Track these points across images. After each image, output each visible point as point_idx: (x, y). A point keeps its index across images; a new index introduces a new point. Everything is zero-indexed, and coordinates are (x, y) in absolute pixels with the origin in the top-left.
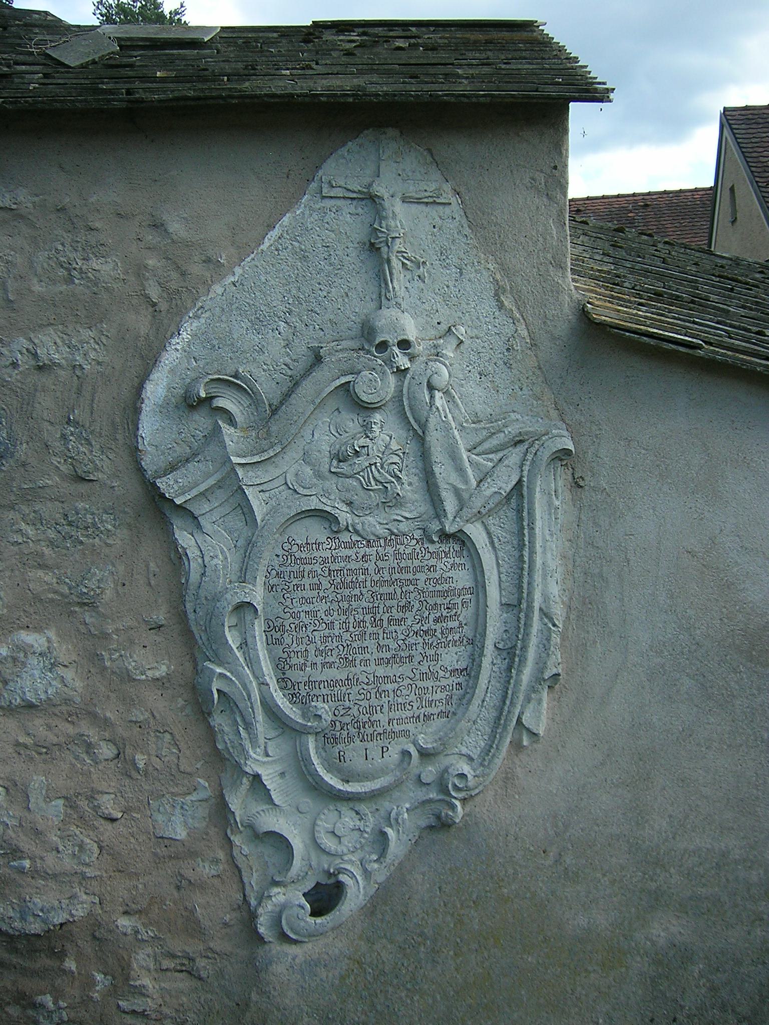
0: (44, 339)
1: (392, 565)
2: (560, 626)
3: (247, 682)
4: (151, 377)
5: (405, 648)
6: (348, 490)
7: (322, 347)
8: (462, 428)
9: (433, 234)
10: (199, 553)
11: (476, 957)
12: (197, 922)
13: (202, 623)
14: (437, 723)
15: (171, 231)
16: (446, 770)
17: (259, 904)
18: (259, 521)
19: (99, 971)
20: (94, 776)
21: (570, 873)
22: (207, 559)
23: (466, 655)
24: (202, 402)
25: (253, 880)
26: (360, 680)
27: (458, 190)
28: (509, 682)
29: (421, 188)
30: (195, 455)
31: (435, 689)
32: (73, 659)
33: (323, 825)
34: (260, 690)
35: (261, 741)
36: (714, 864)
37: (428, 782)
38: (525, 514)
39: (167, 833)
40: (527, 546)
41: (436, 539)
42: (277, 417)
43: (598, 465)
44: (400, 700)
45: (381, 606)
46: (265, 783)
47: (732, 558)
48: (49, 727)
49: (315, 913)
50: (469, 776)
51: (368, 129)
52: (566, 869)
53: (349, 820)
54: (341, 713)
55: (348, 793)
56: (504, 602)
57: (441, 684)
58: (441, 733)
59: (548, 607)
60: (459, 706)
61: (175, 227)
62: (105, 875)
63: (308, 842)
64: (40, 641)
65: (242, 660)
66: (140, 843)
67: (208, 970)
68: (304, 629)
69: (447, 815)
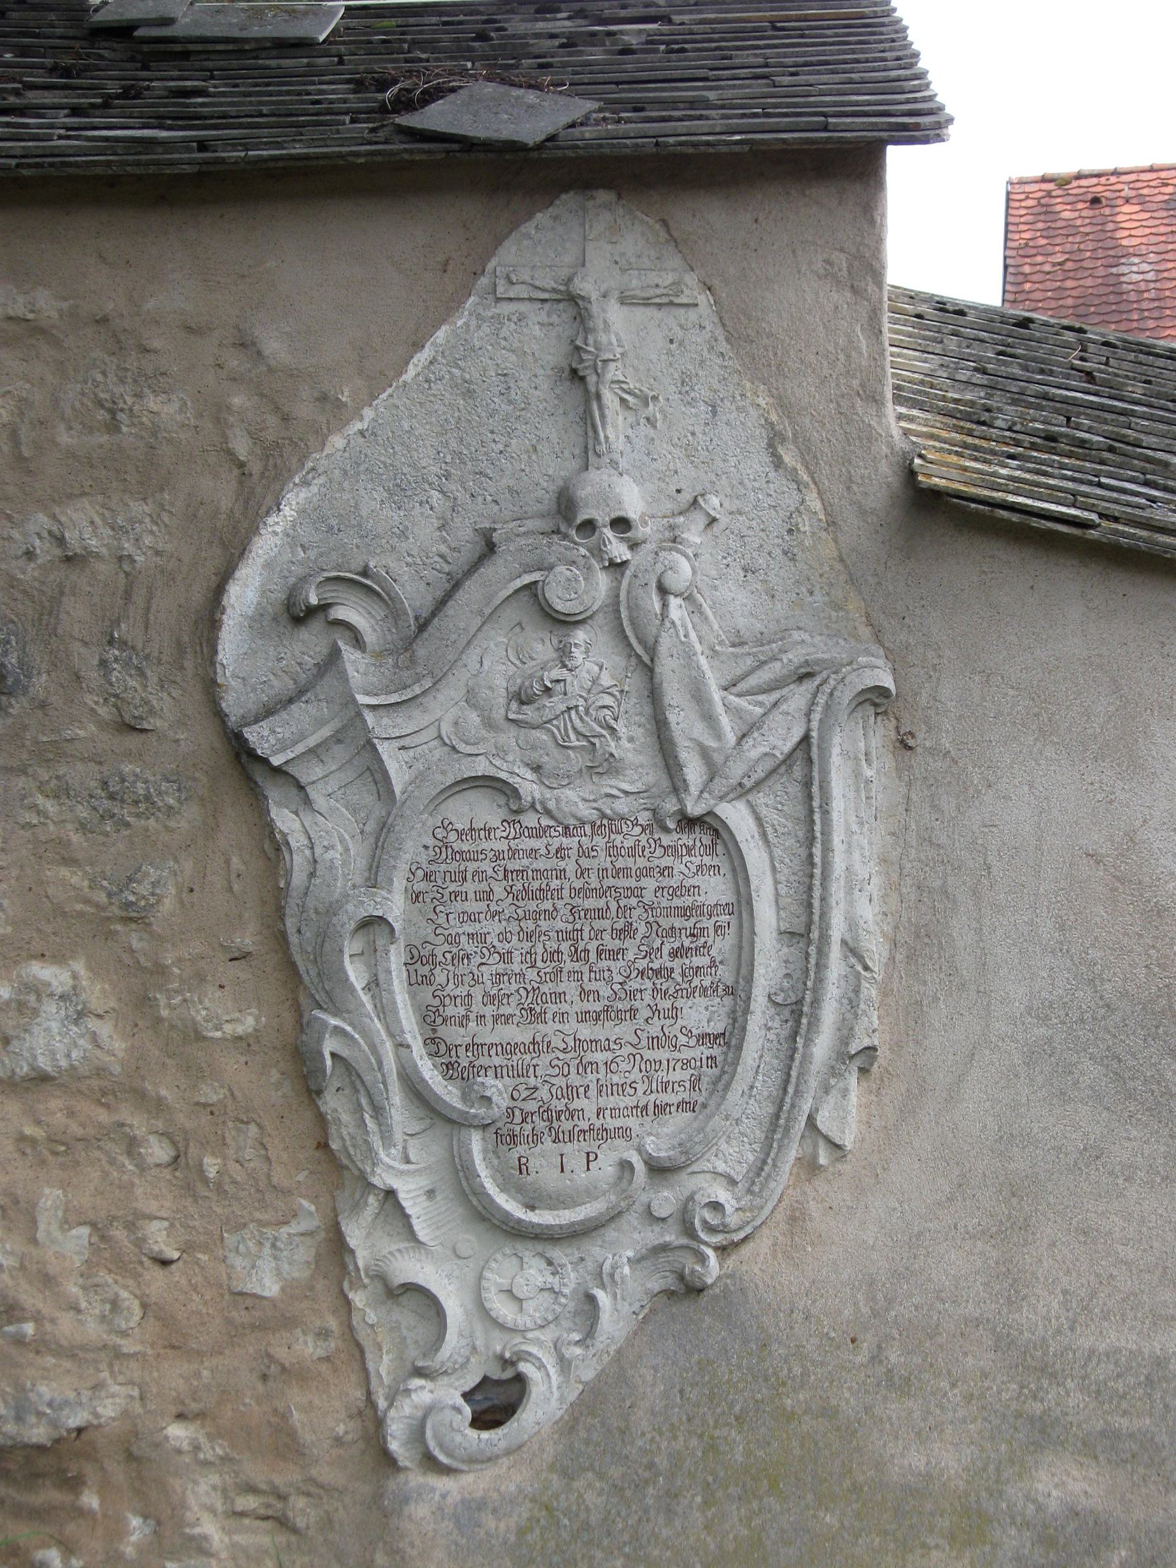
0: (75, 516)
1: (603, 865)
2: (876, 970)
3: (377, 1041)
4: (238, 574)
5: (623, 996)
6: (534, 748)
7: (495, 530)
8: (714, 654)
9: (669, 353)
10: (306, 842)
11: (738, 1509)
12: (292, 1434)
13: (309, 949)
14: (677, 1121)
15: (266, 353)
16: (691, 1198)
17: (391, 1405)
18: (398, 789)
19: (136, 1512)
20: (139, 1191)
21: (896, 1379)
22: (318, 850)
23: (723, 1011)
24: (312, 612)
25: (383, 1367)
26: (553, 1045)
27: (709, 284)
28: (792, 1058)
29: (651, 283)
30: (302, 692)
31: (672, 1064)
32: (112, 1005)
33: (495, 1279)
34: (398, 1057)
35: (398, 1137)
36: (1142, 1378)
37: (663, 1215)
38: (815, 789)
39: (249, 1286)
40: (819, 840)
41: (671, 825)
42: (425, 635)
43: (938, 714)
44: (616, 1079)
45: (587, 929)
46: (404, 1204)
47: (1165, 867)
48: (71, 1114)
49: (482, 1421)
50: (727, 1207)
51: (567, 192)
52: (889, 1371)
53: (535, 1273)
54: (523, 1096)
55: (533, 1225)
56: (783, 929)
57: (682, 1056)
58: (683, 1136)
59: (856, 939)
60: (711, 1094)
61: (274, 347)
62: (150, 1352)
63: (470, 1307)
64: (62, 978)
65: (369, 1007)
66: (206, 1303)
67: (308, 1515)
68: (466, 961)
69: (693, 1271)
